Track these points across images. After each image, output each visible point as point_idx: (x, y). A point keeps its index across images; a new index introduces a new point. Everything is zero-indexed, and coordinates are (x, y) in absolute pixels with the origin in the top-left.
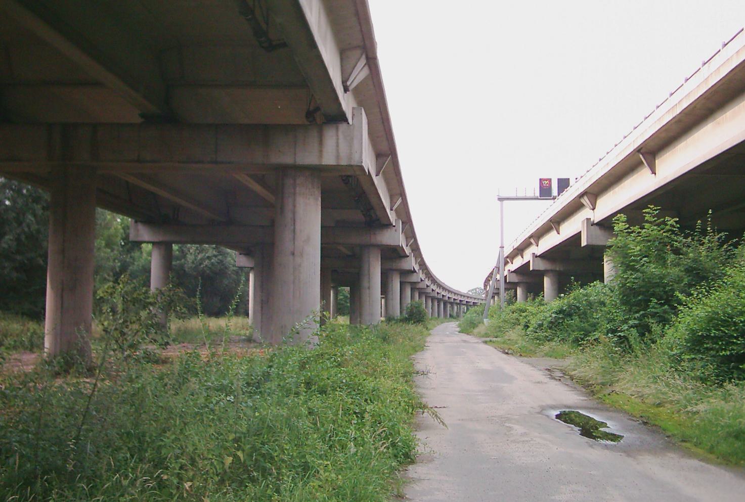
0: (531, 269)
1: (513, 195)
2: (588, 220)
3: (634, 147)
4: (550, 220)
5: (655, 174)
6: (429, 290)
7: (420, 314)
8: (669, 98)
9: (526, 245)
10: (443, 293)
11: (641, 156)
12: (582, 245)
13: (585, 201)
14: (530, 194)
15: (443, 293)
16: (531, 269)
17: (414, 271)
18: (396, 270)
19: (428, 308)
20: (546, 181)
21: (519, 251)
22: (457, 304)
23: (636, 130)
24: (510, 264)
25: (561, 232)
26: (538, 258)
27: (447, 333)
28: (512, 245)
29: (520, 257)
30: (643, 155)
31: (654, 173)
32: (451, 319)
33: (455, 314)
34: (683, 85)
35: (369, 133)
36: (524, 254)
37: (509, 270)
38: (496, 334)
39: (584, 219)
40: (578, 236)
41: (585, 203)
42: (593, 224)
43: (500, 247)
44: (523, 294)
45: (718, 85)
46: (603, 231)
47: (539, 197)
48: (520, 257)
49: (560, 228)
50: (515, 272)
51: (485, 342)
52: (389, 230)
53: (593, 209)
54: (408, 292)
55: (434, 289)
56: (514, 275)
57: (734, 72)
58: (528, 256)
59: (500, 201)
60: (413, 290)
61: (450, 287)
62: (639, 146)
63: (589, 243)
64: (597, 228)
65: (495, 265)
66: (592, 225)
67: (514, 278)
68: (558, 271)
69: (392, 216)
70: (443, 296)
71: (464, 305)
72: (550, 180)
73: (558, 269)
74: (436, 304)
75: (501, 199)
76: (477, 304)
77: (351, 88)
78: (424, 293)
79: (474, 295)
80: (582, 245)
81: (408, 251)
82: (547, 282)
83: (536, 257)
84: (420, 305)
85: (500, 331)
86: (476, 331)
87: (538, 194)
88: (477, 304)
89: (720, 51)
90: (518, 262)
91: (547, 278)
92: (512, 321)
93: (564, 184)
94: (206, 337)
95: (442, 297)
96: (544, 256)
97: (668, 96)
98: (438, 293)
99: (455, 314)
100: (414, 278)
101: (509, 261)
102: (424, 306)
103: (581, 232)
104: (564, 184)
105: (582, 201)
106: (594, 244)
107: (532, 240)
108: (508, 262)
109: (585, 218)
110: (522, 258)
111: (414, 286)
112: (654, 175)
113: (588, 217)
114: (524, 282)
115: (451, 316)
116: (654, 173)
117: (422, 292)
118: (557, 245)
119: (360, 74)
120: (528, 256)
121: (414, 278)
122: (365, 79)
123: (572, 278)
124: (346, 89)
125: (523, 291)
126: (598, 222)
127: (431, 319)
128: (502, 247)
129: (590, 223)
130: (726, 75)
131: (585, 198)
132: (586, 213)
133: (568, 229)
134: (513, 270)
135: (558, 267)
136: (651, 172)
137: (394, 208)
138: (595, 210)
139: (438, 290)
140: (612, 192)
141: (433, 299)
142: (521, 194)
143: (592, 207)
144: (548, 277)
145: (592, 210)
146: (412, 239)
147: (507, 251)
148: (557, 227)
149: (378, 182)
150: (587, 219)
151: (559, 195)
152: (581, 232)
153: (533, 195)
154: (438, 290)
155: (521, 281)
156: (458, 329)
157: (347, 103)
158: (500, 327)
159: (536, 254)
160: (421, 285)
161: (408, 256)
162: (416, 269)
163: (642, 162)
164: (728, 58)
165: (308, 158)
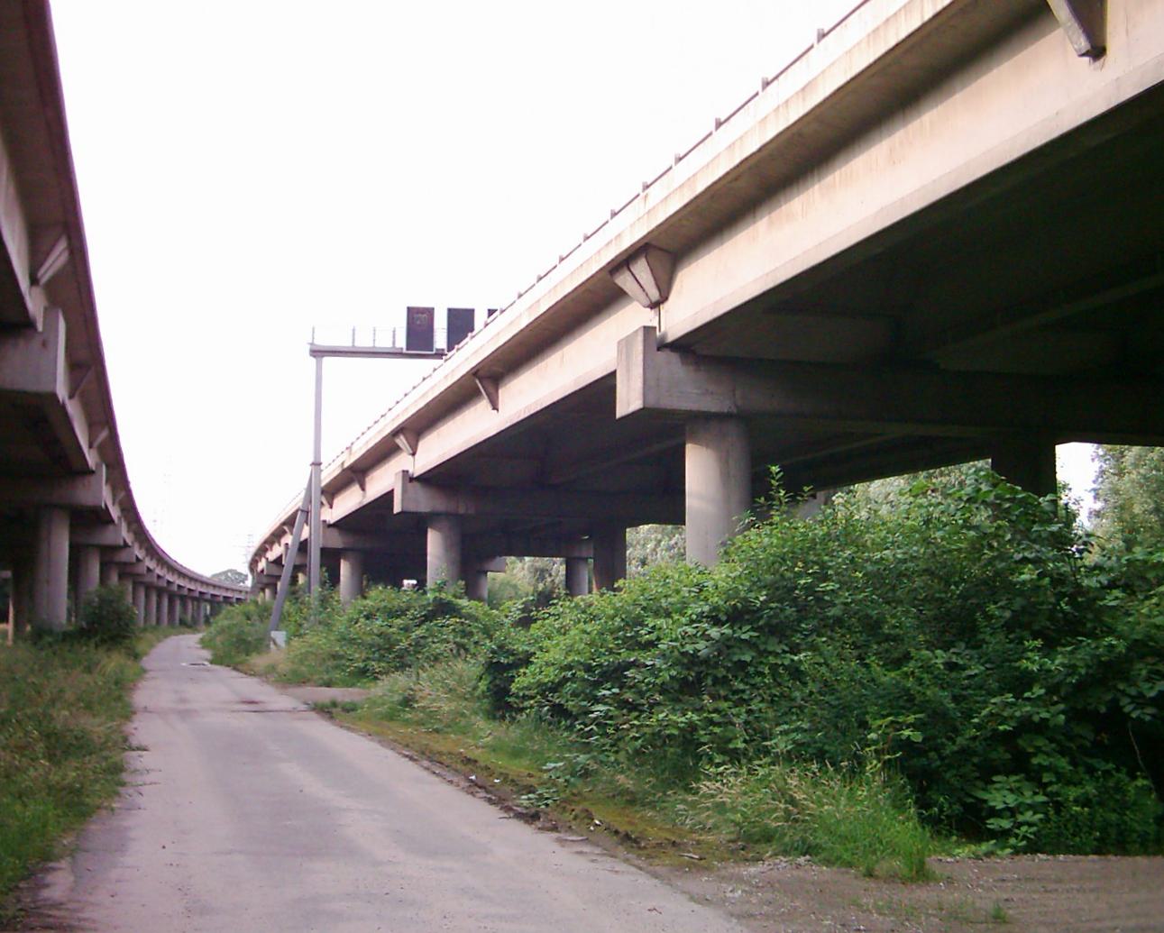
1: (345, 343)
2: (405, 472)
3: (922, 17)
4: (475, 373)
5: (498, 410)
6: (141, 569)
7: (120, 619)
8: (610, 221)
9: (383, 452)
10: (170, 577)
11: (477, 382)
12: (621, 411)
13: (401, 441)
14: (384, 343)
15: (170, 577)
17: (126, 545)
18: (61, 507)
19: (139, 608)
20: (423, 313)
21: (356, 473)
22: (194, 599)
23: (587, 241)
25: (500, 407)
26: (416, 484)
27: (184, 664)
28: (339, 462)
31: (495, 408)
32: (182, 629)
33: (189, 618)
34: (671, 168)
35: (67, 348)
36: (367, 479)
38: (326, 677)
39: (637, 328)
40: (604, 388)
41: (401, 445)
42: (663, 346)
43: (313, 464)
44: (353, 574)
46: (691, 368)
47: (405, 351)
49: (500, 391)
50: (338, 525)
51: (327, 711)
52: (21, 342)
53: (414, 454)
54: (94, 569)
55: (151, 567)
56: (334, 533)
57: (689, 209)
59: (314, 357)
60: (105, 567)
61: (185, 568)
62: (642, 238)
63: (652, 403)
64: (674, 358)
65: (300, 504)
66: (659, 349)
67: (336, 541)
68: (462, 515)
69: (91, 458)
70: (169, 582)
71: (206, 601)
72: (429, 312)
73: (462, 511)
74: (154, 598)
75: (318, 353)
76: (231, 600)
77: (44, 280)
78: (142, 583)
79: (227, 584)
80: (621, 411)
81: (115, 512)
82: (434, 542)
83: (412, 479)
84: (122, 594)
85: (337, 667)
86: (259, 661)
87: (401, 343)
88: (231, 600)
89: (671, 168)
90: (349, 502)
91: (434, 532)
92: (369, 639)
93: (461, 323)
95: (165, 585)
96: (434, 479)
97: (672, 162)
98: (159, 577)
99: (189, 618)
102: (130, 599)
103: (393, 490)
104: (461, 323)
105: (398, 441)
106: (663, 407)
110: (363, 489)
111: (109, 553)
113: (405, 469)
114: (352, 550)
115: (183, 623)
116: (495, 408)
117: (138, 581)
119: (58, 258)
120: (383, 480)
121: (108, 537)
122: (64, 267)
123: (775, 469)
124: (34, 281)
125: (725, 476)
126: (421, 475)
127: (145, 630)
128: (317, 464)
129: (655, 343)
130: (548, 310)
131: (402, 437)
132: (629, 319)
134: (332, 522)
135: (761, 399)
136: (1084, 44)
137: (96, 444)
138: (416, 456)
139: (158, 571)
140: (817, 187)
141: (149, 588)
142: (364, 342)
143: (411, 452)
144: (439, 530)
145: (410, 457)
146: (103, 429)
147: (329, 474)
148: (491, 390)
149: (73, 409)
150: (645, 327)
151: (450, 348)
152: (613, 374)
153: (391, 346)
154: (158, 571)
155: (347, 546)
156: (207, 654)
157: (35, 303)
158: (335, 656)
160: (124, 556)
161: (93, 472)
162: (129, 542)
163: (480, 392)
165: (96, 541)
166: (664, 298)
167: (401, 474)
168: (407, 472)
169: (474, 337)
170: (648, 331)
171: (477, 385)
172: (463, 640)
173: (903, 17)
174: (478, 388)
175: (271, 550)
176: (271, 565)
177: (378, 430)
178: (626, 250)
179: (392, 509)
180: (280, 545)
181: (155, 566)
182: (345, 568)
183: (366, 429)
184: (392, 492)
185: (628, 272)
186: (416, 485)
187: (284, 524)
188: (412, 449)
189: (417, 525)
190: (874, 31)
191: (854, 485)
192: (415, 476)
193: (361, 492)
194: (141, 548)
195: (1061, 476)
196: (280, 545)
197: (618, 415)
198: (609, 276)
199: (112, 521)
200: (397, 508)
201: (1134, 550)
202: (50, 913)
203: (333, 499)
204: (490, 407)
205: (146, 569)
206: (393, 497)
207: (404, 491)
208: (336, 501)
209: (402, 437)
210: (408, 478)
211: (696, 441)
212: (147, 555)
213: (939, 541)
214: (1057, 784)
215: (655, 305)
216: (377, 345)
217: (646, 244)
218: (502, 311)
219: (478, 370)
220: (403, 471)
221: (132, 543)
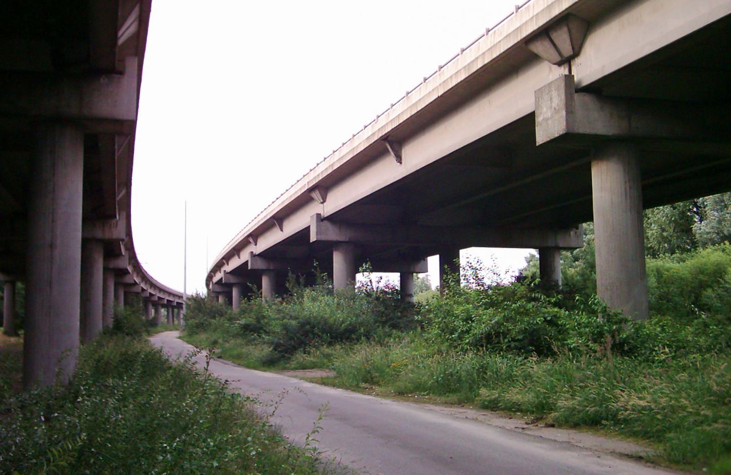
0: (249, 268)
2: (318, 215)
13: (316, 195)
16: (249, 268)
21: (236, 251)
24: (226, 266)
26: (326, 222)
29: (236, 257)
30: (390, 144)
31: (239, 258)
37: (225, 271)
39: (313, 214)
40: (306, 231)
42: (227, 273)
45: (475, 74)
48: (236, 257)
58: (245, 256)
81: (130, 269)
82: (265, 282)
83: (255, 256)
90: (235, 263)
94: (718, 361)
100: (128, 279)
101: (225, 262)
103: (309, 226)
107: (251, 240)
108: (250, 242)
109: (315, 213)
112: (399, 164)
116: (239, 258)
118: (337, 211)
120: (245, 256)
121: (128, 279)
126: (328, 216)
133: (292, 226)
134: (229, 271)
139: (143, 285)
143: (322, 201)
152: (309, 226)
159: (254, 253)
163: (389, 151)
164: (484, 51)
166: (576, 54)
167: (315, 216)
168: (320, 214)
171: (386, 146)
174: (387, 149)
175: (215, 276)
176: (229, 275)
178: (556, 16)
179: (310, 241)
180: (220, 272)
181: (140, 281)
182: (235, 292)
184: (247, 261)
185: (548, 39)
186: (257, 258)
187: (223, 258)
188: (323, 199)
189: (324, 250)
191: (698, 198)
192: (257, 254)
194: (137, 276)
195: (373, 273)
196: (220, 272)
197: (311, 242)
198: (524, 45)
199: (129, 273)
200: (313, 238)
201: (496, 284)
202: (66, 448)
203: (228, 261)
204: (280, 230)
205: (140, 289)
206: (309, 231)
207: (318, 227)
208: (230, 263)
209: (317, 192)
210: (320, 219)
211: (336, 250)
212: (142, 281)
217: (568, 14)
220: (317, 214)
221: (140, 282)
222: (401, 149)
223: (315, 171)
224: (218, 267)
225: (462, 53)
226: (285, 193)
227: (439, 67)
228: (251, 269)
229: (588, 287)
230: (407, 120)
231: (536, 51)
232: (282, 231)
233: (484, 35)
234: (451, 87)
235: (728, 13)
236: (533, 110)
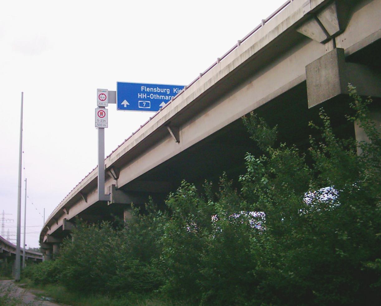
0: (108, 205)
25: (88, 202)
36: (180, 132)
83: (68, 221)
90: (54, 228)
107: (65, 211)
108: (64, 212)
120: (61, 222)
138: (118, 180)
159: (67, 219)
169: (162, 110)
170: (113, 186)
172: (137, 272)
173: (281, 26)
177: (94, 174)
183: (66, 196)
190: (286, 20)
193: (320, 42)
200: (63, 229)
204: (85, 202)
213: (304, 178)
214: (342, 254)
215: (116, 179)
216: (23, 233)
218: (187, 88)
219: (170, 122)
222: (179, 132)
223: (110, 157)
224: (49, 224)
225: (239, 45)
226: (88, 175)
227: (239, 42)
228: (65, 230)
229: (34, 273)
230: (225, 77)
231: (304, 33)
232: (87, 202)
233: (237, 46)
234: (147, 136)
235: (380, 38)
236: (303, 80)
